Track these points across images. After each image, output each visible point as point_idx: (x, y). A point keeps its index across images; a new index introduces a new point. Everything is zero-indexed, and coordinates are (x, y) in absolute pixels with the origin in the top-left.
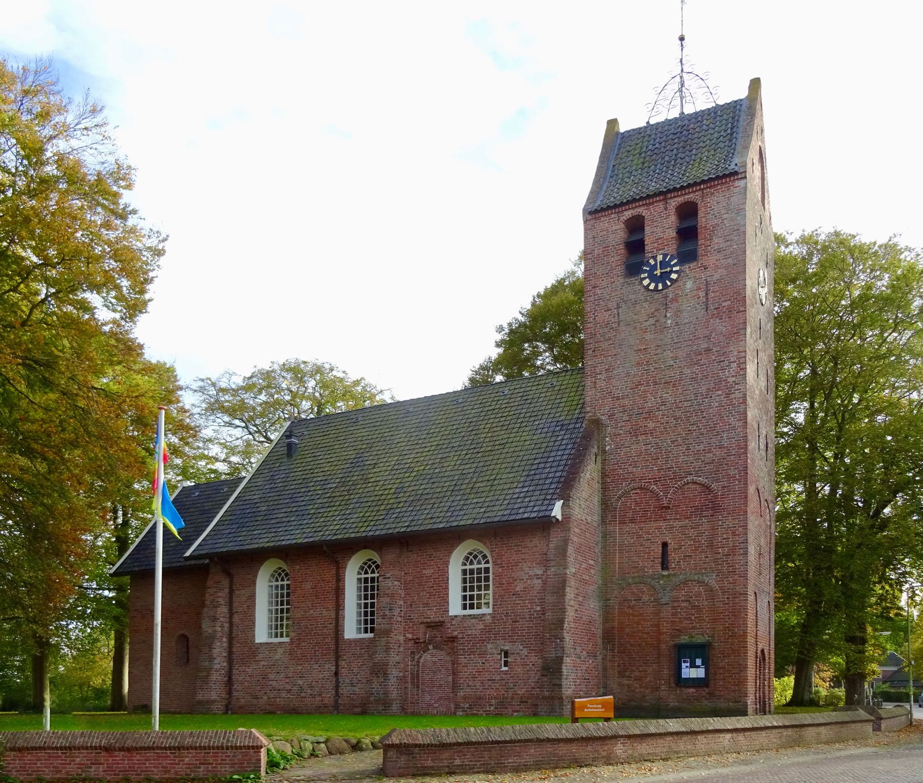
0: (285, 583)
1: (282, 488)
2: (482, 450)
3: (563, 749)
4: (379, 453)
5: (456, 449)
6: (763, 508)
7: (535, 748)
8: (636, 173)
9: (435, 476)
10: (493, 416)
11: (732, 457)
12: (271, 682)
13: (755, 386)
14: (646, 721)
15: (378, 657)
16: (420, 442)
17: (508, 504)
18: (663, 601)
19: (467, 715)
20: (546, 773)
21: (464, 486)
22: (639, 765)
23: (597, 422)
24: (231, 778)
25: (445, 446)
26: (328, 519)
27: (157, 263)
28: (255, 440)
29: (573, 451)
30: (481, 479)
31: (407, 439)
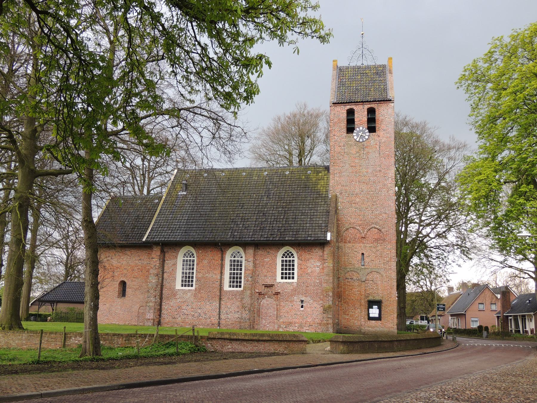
12: (183, 311)
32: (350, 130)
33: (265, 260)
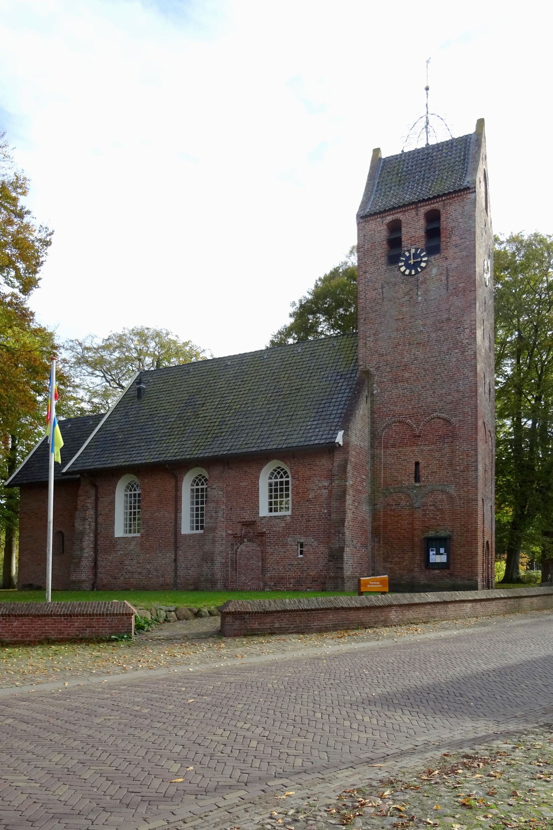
0: (137, 492)
1: (134, 422)
2: (283, 393)
3: (353, 615)
4: (206, 395)
5: (263, 392)
6: (487, 437)
7: (333, 615)
8: (394, 188)
9: (248, 412)
10: (290, 368)
11: (466, 399)
12: (126, 567)
13: (482, 346)
14: (412, 594)
15: (207, 548)
16: (236, 387)
17: (303, 433)
18: (416, 505)
19: (273, 590)
20: (341, 633)
21: (270, 420)
22: (407, 627)
23: (367, 373)
24: (110, 637)
25: (255, 390)
26: (169, 445)
27: (45, 251)
28: (110, 386)
29: (350, 394)
30: (282, 415)
31: (226, 385)
33: (241, 484)
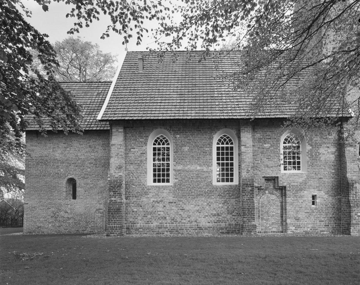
32: (31, 17)
33: (265, 145)
